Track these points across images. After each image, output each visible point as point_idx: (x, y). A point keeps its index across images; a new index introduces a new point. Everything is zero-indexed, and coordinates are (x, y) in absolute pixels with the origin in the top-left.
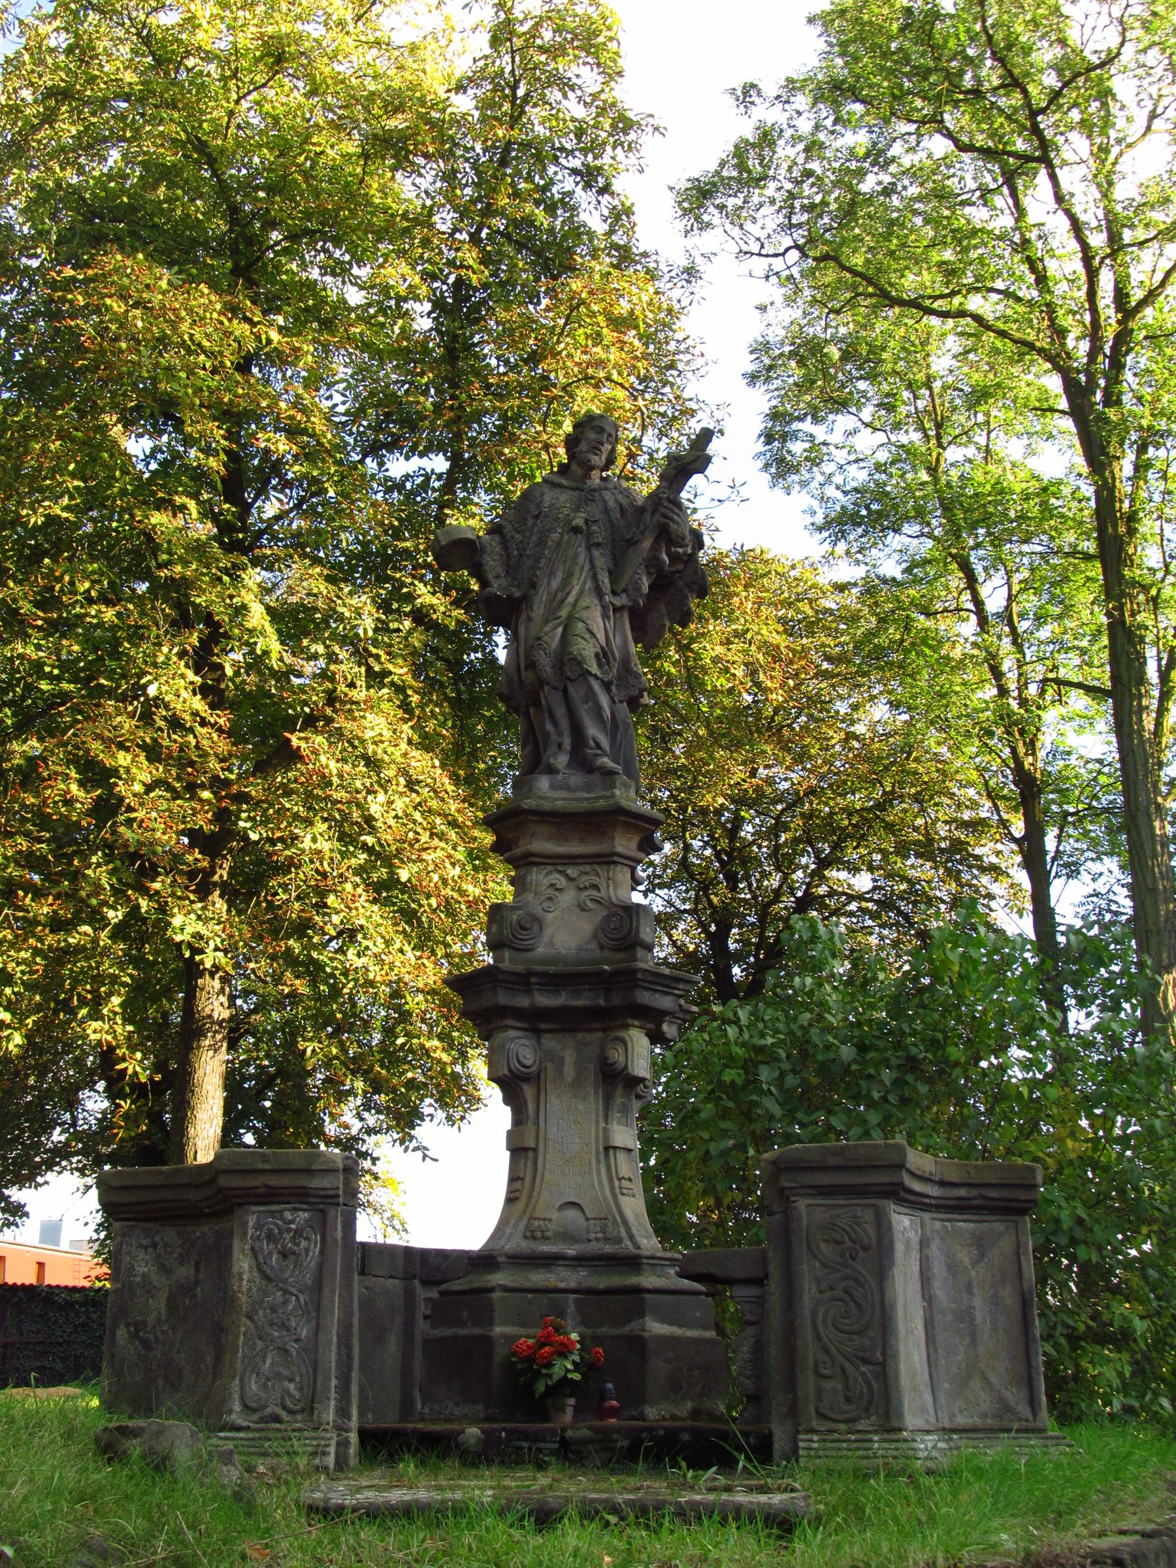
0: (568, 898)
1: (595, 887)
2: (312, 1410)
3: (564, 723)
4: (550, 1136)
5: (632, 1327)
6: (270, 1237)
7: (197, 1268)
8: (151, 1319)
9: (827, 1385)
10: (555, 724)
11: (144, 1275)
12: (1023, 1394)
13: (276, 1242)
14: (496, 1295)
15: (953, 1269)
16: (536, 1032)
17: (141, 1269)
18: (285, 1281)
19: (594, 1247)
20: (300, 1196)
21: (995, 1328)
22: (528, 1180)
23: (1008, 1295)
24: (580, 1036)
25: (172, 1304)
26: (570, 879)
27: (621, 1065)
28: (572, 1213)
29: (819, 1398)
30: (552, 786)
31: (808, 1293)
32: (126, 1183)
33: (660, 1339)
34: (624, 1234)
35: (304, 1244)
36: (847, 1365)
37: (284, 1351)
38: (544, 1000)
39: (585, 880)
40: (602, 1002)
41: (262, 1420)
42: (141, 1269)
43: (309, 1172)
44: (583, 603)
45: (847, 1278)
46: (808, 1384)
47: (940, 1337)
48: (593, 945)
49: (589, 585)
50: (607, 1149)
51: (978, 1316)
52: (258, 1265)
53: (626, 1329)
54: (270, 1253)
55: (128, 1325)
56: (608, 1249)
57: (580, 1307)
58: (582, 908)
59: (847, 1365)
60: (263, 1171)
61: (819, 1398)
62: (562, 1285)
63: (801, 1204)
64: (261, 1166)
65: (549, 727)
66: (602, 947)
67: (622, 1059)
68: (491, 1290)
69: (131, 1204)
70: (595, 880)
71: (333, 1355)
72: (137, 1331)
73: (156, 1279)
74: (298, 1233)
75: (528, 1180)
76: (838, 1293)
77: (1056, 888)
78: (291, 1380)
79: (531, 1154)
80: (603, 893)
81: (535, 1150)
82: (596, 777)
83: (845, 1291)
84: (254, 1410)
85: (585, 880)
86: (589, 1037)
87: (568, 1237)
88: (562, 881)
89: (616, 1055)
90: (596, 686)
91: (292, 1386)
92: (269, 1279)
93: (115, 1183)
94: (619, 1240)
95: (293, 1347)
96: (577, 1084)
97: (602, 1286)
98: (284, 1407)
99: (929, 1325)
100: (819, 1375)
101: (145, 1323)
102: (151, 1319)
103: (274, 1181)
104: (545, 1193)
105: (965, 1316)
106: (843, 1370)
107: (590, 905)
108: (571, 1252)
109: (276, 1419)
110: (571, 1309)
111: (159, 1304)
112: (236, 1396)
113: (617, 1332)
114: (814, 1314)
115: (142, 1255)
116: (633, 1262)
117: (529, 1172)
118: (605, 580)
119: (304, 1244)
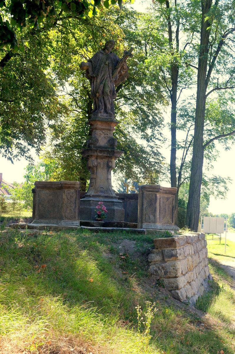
3: (103, 104)
5: (113, 207)
10: (101, 103)
12: (171, 220)
14: (91, 202)
15: (163, 202)
21: (168, 211)
22: (95, 183)
23: (171, 206)
26: (103, 132)
27: (111, 166)
30: (101, 115)
33: (117, 209)
39: (106, 133)
44: (107, 80)
47: (161, 212)
48: (107, 145)
49: (108, 76)
50: (107, 179)
51: (166, 209)
58: (105, 138)
65: (100, 104)
66: (108, 145)
68: (90, 201)
71: (139, 208)
75: (95, 183)
77: (178, 132)
81: (96, 178)
88: (101, 133)
96: (103, 168)
97: (87, 200)
99: (160, 210)
105: (165, 209)
114: (145, 208)
118: (111, 75)
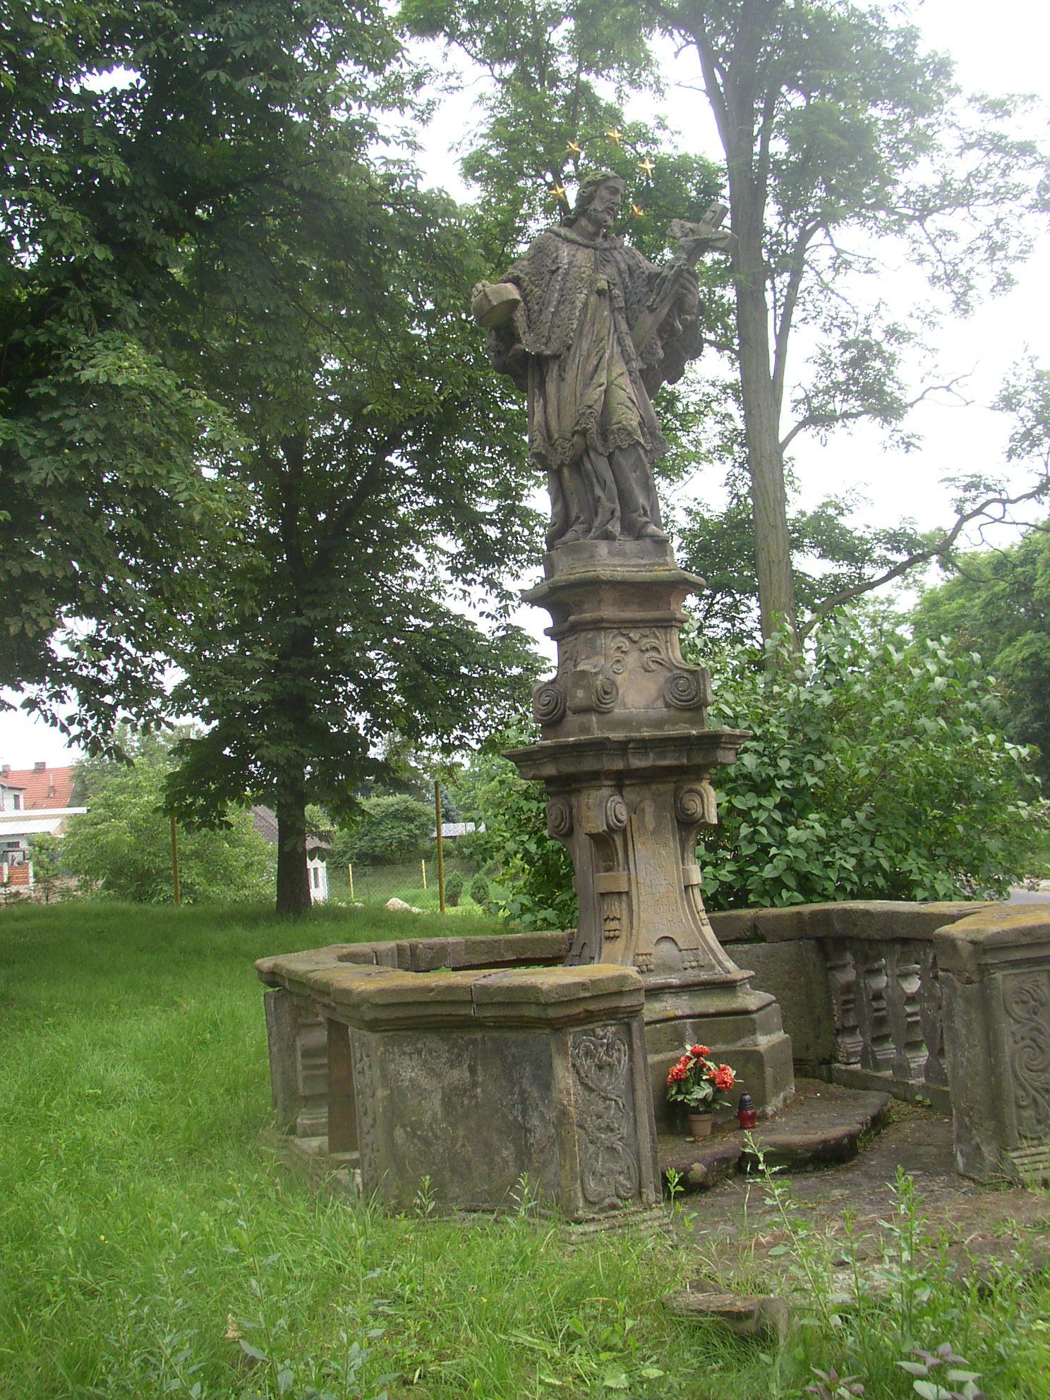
0: (632, 659)
1: (655, 649)
2: (640, 1193)
4: (641, 880)
6: (588, 1053)
7: (472, 1070)
8: (427, 1118)
9: (1026, 1113)
11: (411, 1080)
13: (593, 1057)
16: (619, 788)
17: (408, 1074)
18: (605, 1090)
19: (692, 976)
20: (612, 1014)
24: (654, 787)
25: (447, 1103)
28: (666, 946)
29: (1020, 1124)
30: (610, 553)
31: (1008, 1046)
32: (391, 1000)
34: (714, 961)
35: (616, 1055)
36: (1037, 1096)
37: (611, 1149)
38: (637, 763)
40: (685, 761)
41: (602, 1210)
42: (408, 1074)
43: (620, 993)
45: (1032, 1029)
46: (1011, 1112)
48: (660, 703)
50: (686, 887)
52: (581, 1079)
53: (737, 1046)
54: (590, 1067)
55: (404, 1126)
56: (704, 976)
57: (696, 1028)
59: (1037, 1096)
60: (584, 999)
61: (1020, 1124)
62: (680, 1013)
63: (999, 975)
64: (583, 995)
66: (668, 706)
67: (699, 810)
69: (398, 1019)
70: (653, 642)
72: (414, 1131)
73: (425, 1082)
74: (610, 1046)
76: (1028, 1042)
78: (620, 1173)
79: (624, 897)
80: (663, 656)
82: (647, 543)
83: (1032, 1039)
84: (594, 1203)
85: (646, 643)
86: (663, 788)
87: (668, 968)
89: (694, 806)
90: (642, 452)
91: (621, 1178)
92: (591, 1090)
93: (380, 1001)
94: (713, 967)
95: (619, 1146)
97: (712, 1010)
98: (619, 1196)
100: (1020, 1107)
101: (421, 1123)
102: (427, 1118)
103: (592, 1006)
104: (644, 931)
106: (1034, 1100)
107: (654, 666)
108: (675, 981)
109: (613, 1207)
110: (689, 1032)
111: (435, 1104)
112: (580, 1195)
113: (731, 1048)
114: (1012, 1057)
115: (407, 1061)
116: (728, 986)
117: (625, 913)
119: (616, 1055)
